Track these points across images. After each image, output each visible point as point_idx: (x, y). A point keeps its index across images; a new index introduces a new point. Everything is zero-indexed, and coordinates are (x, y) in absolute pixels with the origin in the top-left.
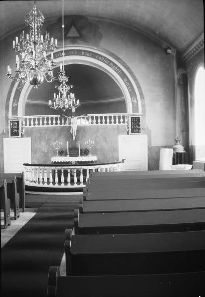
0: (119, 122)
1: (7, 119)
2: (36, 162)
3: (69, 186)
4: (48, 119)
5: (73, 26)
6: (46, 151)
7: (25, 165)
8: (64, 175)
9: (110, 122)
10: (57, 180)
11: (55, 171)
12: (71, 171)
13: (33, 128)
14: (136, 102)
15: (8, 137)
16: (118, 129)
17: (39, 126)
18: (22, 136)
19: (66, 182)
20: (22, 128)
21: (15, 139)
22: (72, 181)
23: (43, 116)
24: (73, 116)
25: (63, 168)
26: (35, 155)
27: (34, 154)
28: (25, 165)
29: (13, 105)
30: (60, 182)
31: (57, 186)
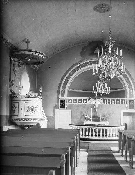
1: (58, 99)
2: (74, 124)
3: (98, 138)
4: (79, 100)
5: (97, 48)
6: (80, 118)
7: (69, 125)
8: (91, 132)
9: (112, 103)
10: (87, 134)
11: (83, 128)
12: (95, 129)
14: (132, 92)
15: (58, 109)
18: (67, 109)
19: (92, 135)
20: (67, 104)
21: (62, 110)
22: (96, 135)
24: (96, 99)
25: (90, 127)
26: (73, 120)
28: (69, 125)
29: (62, 91)
30: (89, 135)
31: (87, 137)
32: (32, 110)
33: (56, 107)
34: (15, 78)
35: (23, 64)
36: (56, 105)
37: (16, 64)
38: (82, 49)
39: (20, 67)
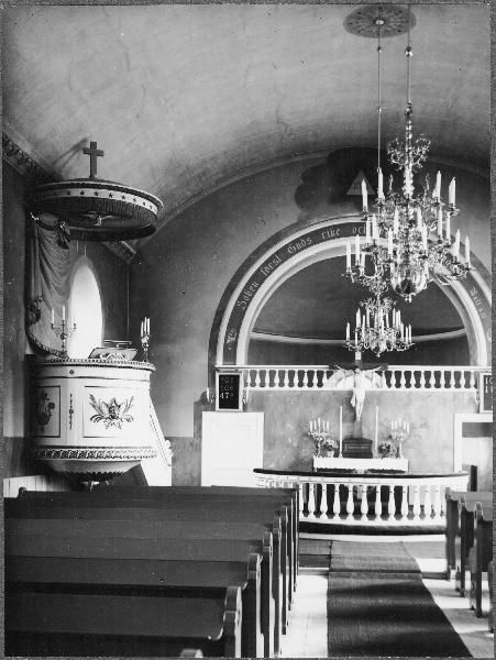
0: (458, 386)
2: (272, 467)
6: (295, 445)
7: (257, 471)
10: (324, 507)
13: (269, 392)
15: (214, 410)
16: (454, 399)
17: (292, 389)
18: (245, 409)
19: (344, 513)
20: (245, 392)
23: (428, 368)
24: (357, 370)
25: (337, 481)
26: (271, 452)
27: (269, 449)
28: (257, 471)
32: (111, 413)
33: (204, 404)
34: (47, 291)
35: (74, 236)
36: (204, 394)
37: (50, 237)
38: (304, 178)
39: (66, 247)
